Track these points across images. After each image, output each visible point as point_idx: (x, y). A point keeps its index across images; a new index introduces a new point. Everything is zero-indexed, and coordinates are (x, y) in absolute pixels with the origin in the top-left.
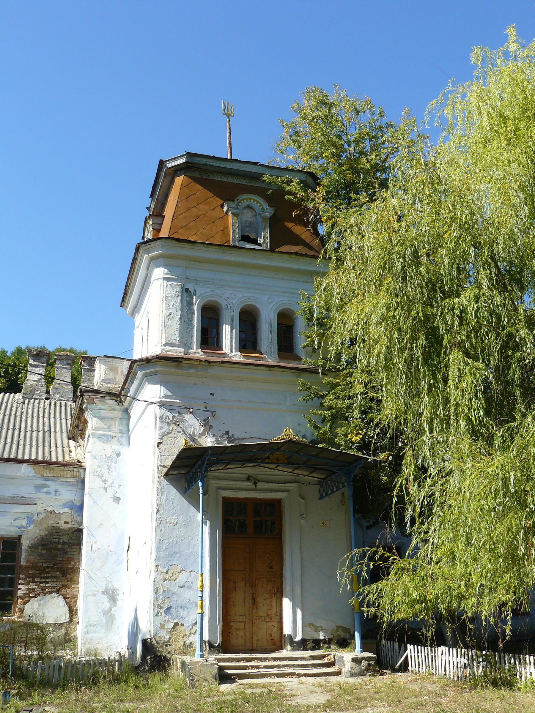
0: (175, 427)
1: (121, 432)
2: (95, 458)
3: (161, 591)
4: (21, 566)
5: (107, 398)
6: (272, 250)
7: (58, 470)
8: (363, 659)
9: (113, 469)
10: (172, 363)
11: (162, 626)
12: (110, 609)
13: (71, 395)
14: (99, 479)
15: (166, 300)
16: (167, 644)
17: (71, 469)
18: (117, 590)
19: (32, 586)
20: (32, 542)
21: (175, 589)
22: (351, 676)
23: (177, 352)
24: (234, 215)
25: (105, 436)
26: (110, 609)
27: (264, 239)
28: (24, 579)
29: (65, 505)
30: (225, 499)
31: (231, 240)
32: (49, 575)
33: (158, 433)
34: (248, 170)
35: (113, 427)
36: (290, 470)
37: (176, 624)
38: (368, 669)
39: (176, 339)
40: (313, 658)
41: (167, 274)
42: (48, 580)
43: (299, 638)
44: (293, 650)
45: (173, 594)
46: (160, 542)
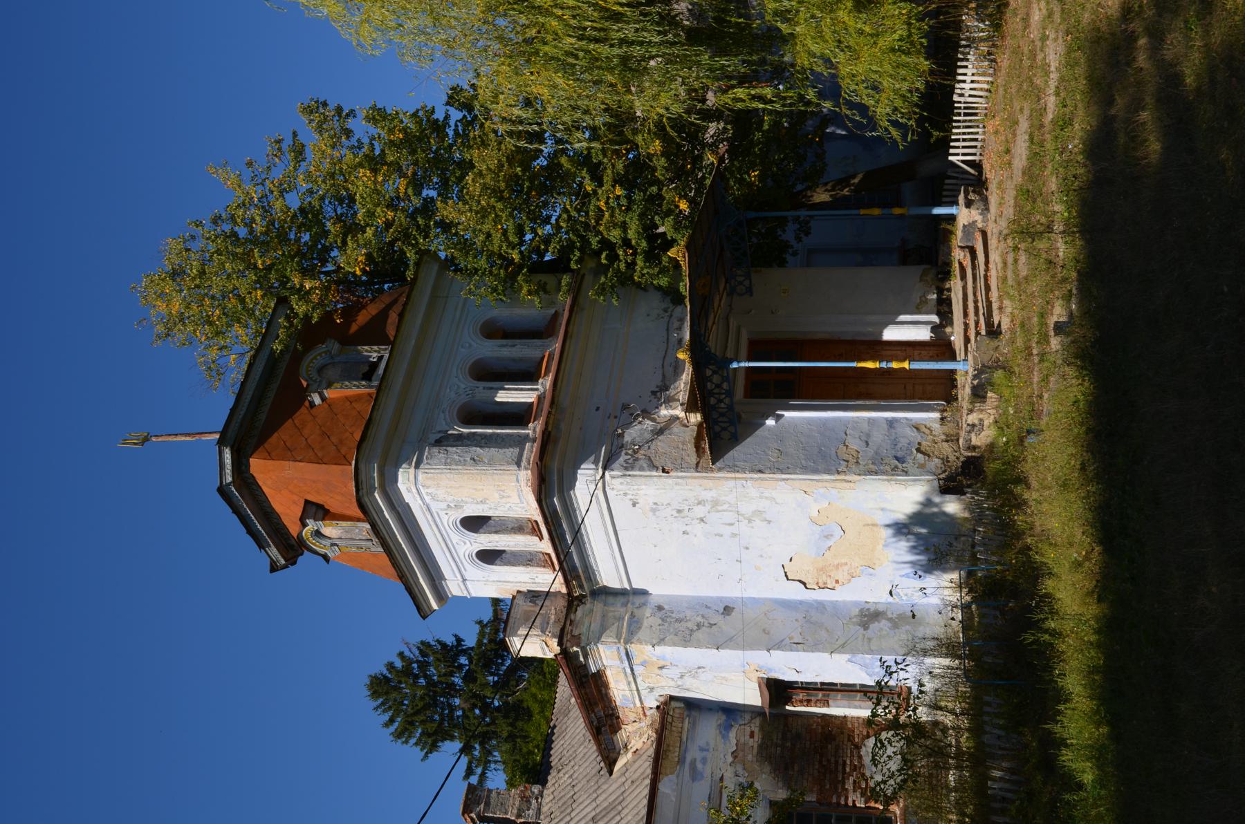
0: (642, 452)
1: (625, 605)
2: (663, 639)
3: (873, 467)
4: (818, 801)
5: (572, 617)
6: (393, 344)
7: (671, 739)
8: (966, 197)
9: (681, 616)
10: (550, 447)
11: (922, 466)
12: (890, 620)
14: (695, 634)
15: (450, 464)
16: (945, 460)
17: (670, 719)
18: (861, 611)
19: (849, 785)
20: (780, 784)
21: (871, 451)
22: (987, 209)
23: (531, 451)
24: (329, 386)
25: (629, 625)
26: (890, 620)
27: (373, 353)
28: (839, 797)
29: (725, 737)
30: (745, 396)
31: (368, 390)
32: (833, 760)
33: (648, 473)
34: (259, 374)
35: (617, 614)
36: (717, 298)
37: (918, 450)
38: (980, 194)
39: (512, 452)
40: (963, 277)
41: (410, 464)
42: (840, 761)
43: (935, 318)
44: (951, 324)
45: (876, 453)
46: (805, 470)
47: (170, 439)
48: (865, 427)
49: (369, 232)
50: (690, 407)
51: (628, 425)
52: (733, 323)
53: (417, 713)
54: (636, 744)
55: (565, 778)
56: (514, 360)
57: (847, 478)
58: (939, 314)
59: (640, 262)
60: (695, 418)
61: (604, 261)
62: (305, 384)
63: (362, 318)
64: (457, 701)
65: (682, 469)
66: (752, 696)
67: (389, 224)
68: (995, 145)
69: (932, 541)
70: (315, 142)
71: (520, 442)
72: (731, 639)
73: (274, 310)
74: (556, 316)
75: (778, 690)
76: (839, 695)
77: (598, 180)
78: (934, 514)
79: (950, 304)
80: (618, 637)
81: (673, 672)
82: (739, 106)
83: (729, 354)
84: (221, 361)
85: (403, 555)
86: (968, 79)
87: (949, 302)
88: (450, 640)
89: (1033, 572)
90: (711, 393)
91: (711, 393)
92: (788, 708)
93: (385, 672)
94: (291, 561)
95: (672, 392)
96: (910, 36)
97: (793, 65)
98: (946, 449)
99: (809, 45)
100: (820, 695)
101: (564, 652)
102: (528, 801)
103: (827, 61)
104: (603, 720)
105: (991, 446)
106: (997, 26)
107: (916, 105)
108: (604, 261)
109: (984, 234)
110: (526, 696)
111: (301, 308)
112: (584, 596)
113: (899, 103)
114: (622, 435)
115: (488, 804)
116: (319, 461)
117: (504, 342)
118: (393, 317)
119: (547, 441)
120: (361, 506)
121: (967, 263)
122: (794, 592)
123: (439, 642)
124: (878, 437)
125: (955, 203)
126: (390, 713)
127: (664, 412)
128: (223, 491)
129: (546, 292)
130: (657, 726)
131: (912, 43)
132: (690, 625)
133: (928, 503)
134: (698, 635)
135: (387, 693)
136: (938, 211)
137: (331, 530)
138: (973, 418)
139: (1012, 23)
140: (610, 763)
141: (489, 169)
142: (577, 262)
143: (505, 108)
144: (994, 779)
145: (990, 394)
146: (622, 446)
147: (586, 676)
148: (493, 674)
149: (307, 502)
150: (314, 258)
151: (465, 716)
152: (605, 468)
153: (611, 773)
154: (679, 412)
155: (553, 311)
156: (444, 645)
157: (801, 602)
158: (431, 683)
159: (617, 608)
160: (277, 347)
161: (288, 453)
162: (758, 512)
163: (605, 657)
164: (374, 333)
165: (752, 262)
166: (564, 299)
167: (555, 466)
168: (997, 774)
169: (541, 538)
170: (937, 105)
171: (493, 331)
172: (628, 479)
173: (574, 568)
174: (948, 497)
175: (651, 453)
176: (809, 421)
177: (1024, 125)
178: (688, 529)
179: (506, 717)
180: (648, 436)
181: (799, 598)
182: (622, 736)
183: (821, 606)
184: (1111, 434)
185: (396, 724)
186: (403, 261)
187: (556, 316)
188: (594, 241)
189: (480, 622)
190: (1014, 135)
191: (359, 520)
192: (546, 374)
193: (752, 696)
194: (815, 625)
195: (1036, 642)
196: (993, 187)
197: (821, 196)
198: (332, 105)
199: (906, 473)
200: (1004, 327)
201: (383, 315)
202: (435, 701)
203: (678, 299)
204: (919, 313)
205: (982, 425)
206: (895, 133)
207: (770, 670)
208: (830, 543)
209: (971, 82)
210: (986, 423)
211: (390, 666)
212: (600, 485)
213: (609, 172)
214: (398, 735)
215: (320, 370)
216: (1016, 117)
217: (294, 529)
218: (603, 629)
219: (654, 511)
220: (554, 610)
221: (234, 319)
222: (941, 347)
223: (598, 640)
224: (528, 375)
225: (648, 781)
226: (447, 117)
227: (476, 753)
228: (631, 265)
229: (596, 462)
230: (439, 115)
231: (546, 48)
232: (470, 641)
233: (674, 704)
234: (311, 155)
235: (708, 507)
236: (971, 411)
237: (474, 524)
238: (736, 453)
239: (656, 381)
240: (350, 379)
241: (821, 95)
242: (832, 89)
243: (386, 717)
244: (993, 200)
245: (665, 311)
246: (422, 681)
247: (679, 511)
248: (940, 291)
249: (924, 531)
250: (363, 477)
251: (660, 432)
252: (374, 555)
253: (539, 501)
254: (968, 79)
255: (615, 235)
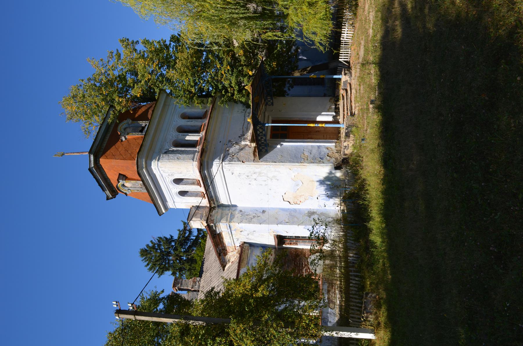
1: (229, 210)
6: (150, 120)
7: (244, 256)
10: (204, 154)
11: (329, 161)
12: (318, 214)
13: (195, 293)
21: (312, 156)
22: (351, 76)
23: (197, 156)
24: (128, 134)
25: (230, 217)
26: (318, 214)
27: (143, 123)
30: (271, 138)
37: (328, 156)
38: (349, 71)
40: (343, 99)
43: (334, 114)
44: (339, 115)
46: (290, 162)
47: (72, 154)
48: (310, 148)
49: (143, 82)
50: (252, 141)
51: (231, 147)
52: (267, 114)
53: (157, 261)
54: (232, 259)
55: (208, 274)
56: (192, 126)
57: (304, 164)
58: (335, 112)
59: (236, 93)
60: (254, 145)
61: (223, 93)
62: (119, 133)
63: (140, 112)
64: (171, 258)
65: (249, 161)
66: (272, 242)
67: (149, 80)
68: (354, 54)
69: (332, 186)
70: (124, 52)
71: (194, 153)
72: (265, 221)
73: (109, 110)
74: (206, 112)
75: (281, 239)
76: (301, 241)
77: (221, 64)
78: (333, 177)
79: (339, 109)
80: (227, 221)
81: (245, 233)
82: (270, 38)
83: (266, 121)
84: (90, 128)
85: (153, 194)
86: (346, 32)
87: (339, 109)
88: (168, 237)
89: (362, 186)
90: (259, 135)
91: (259, 135)
92: (284, 246)
93: (146, 248)
94: (114, 196)
95: (246, 136)
96: (326, 14)
97: (287, 26)
98: (337, 155)
99: (294, 19)
100: (295, 241)
101: (208, 226)
102: (195, 283)
103: (299, 25)
104: (221, 251)
105: (351, 154)
106: (355, 14)
107: (329, 38)
108: (223, 93)
109: (350, 84)
110: (195, 256)
111: (118, 108)
112: (215, 207)
113: (323, 38)
114: (228, 150)
115: (181, 284)
116: (124, 159)
117: (189, 120)
118: (150, 112)
119: (203, 152)
120: (139, 174)
121: (345, 95)
122: (286, 206)
123: (165, 237)
124: (314, 151)
125: (341, 74)
126: (147, 262)
127: (243, 143)
128: (90, 170)
129: (203, 103)
130: (240, 252)
131: (327, 17)
132: (251, 216)
133: (331, 173)
134: (254, 220)
135: (146, 255)
136: (335, 77)
137: (128, 184)
138: (345, 144)
139: (360, 11)
140: (224, 267)
141: (184, 58)
142: (214, 93)
143: (189, 38)
144: (350, 257)
145: (351, 135)
146: (229, 154)
147: (216, 234)
148: (183, 248)
149: (120, 174)
150: (123, 92)
151: (174, 263)
152: (223, 161)
153: (224, 270)
154: (248, 143)
155: (205, 110)
156: (166, 238)
157: (288, 209)
158: (162, 251)
159: (226, 211)
160: (110, 121)
161: (113, 157)
162: (274, 176)
163: (222, 228)
164: (144, 117)
165: (273, 90)
166: (209, 106)
167: (206, 160)
168: (351, 255)
169: (201, 186)
170: (335, 40)
171: (184, 116)
172: (230, 165)
173: (212, 197)
174: (338, 171)
175: (238, 156)
176: (292, 146)
177: (363, 42)
178: (251, 182)
179: (188, 263)
180: (237, 151)
181: (287, 207)
182: (227, 257)
183: (295, 210)
184: (388, 133)
185: (149, 266)
186: (154, 92)
187: (206, 112)
188: (220, 86)
189: (179, 230)
190: (360, 48)
191: (138, 180)
192: (203, 130)
193: (272, 242)
194: (293, 217)
195: (363, 204)
196: (353, 68)
197: (297, 74)
198: (130, 40)
199: (324, 163)
200: (356, 113)
201: (147, 111)
202: (163, 258)
203: (248, 106)
204: (329, 112)
205: (348, 146)
206: (322, 48)
207: (278, 232)
208: (298, 187)
209: (347, 34)
210: (350, 145)
211: (148, 246)
212: (221, 166)
213: (225, 61)
214: (150, 269)
215: (125, 129)
216: (360, 41)
217: (114, 183)
218: (222, 218)
219: (239, 176)
220: (205, 212)
221: (95, 113)
222: (336, 121)
223: (220, 221)
224: (197, 131)
225: (236, 271)
226: (170, 44)
227: (177, 275)
228: (233, 95)
229: (220, 159)
230: (168, 43)
231: (205, 14)
232: (176, 237)
233: (245, 245)
234: (122, 57)
235: (257, 174)
236: (345, 141)
237: (178, 181)
238: (267, 156)
239: (240, 133)
240: (135, 132)
241: (297, 36)
242: (301, 34)
243: (146, 263)
244: (353, 72)
245: (244, 110)
246: (159, 251)
247: (248, 176)
248: (336, 105)
249: (329, 183)
250: (139, 164)
251: (242, 149)
252: (143, 193)
253: (200, 172)
254: (346, 32)
255: (226, 83)
